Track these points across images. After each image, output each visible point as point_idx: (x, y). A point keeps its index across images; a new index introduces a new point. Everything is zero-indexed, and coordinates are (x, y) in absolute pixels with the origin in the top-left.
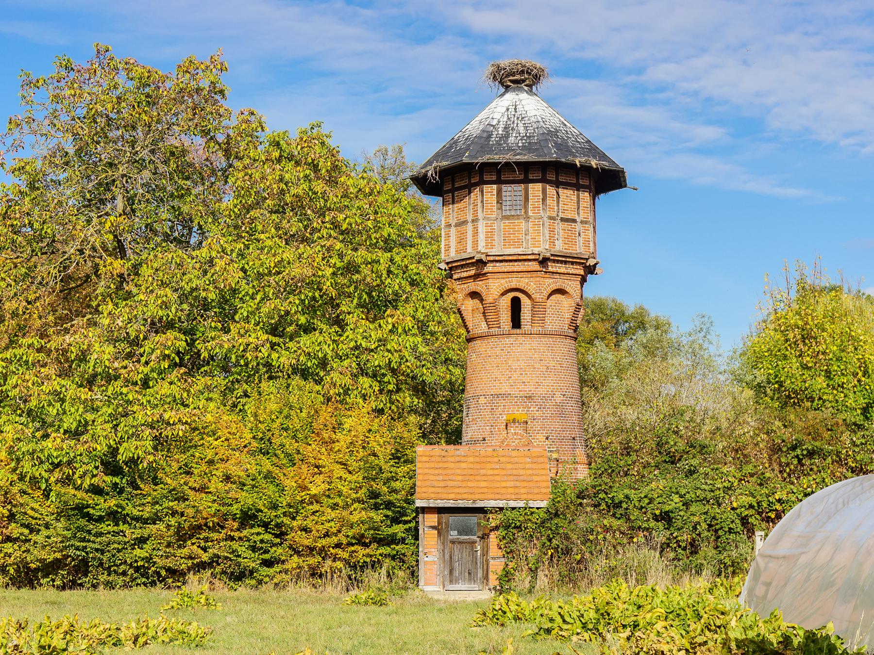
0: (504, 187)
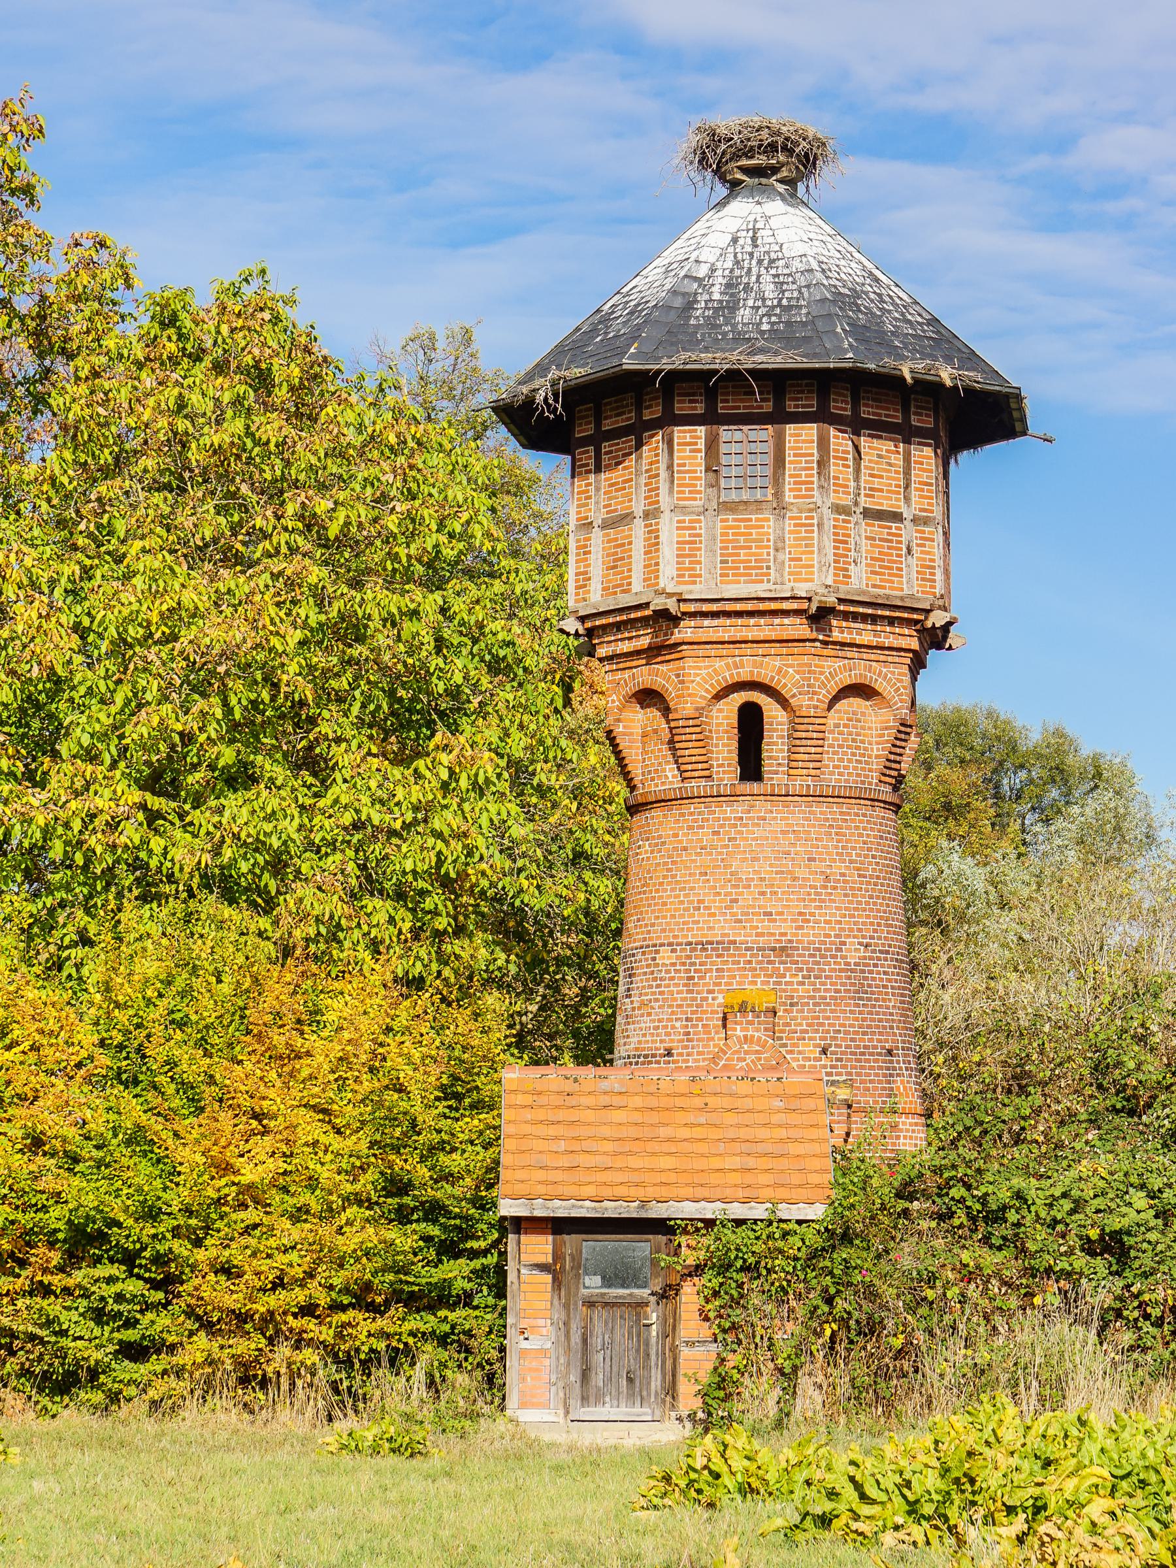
0: (726, 433)
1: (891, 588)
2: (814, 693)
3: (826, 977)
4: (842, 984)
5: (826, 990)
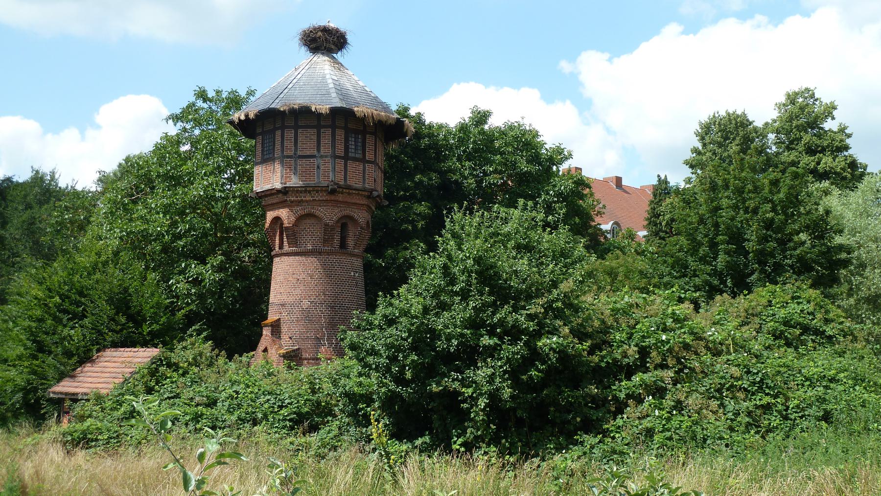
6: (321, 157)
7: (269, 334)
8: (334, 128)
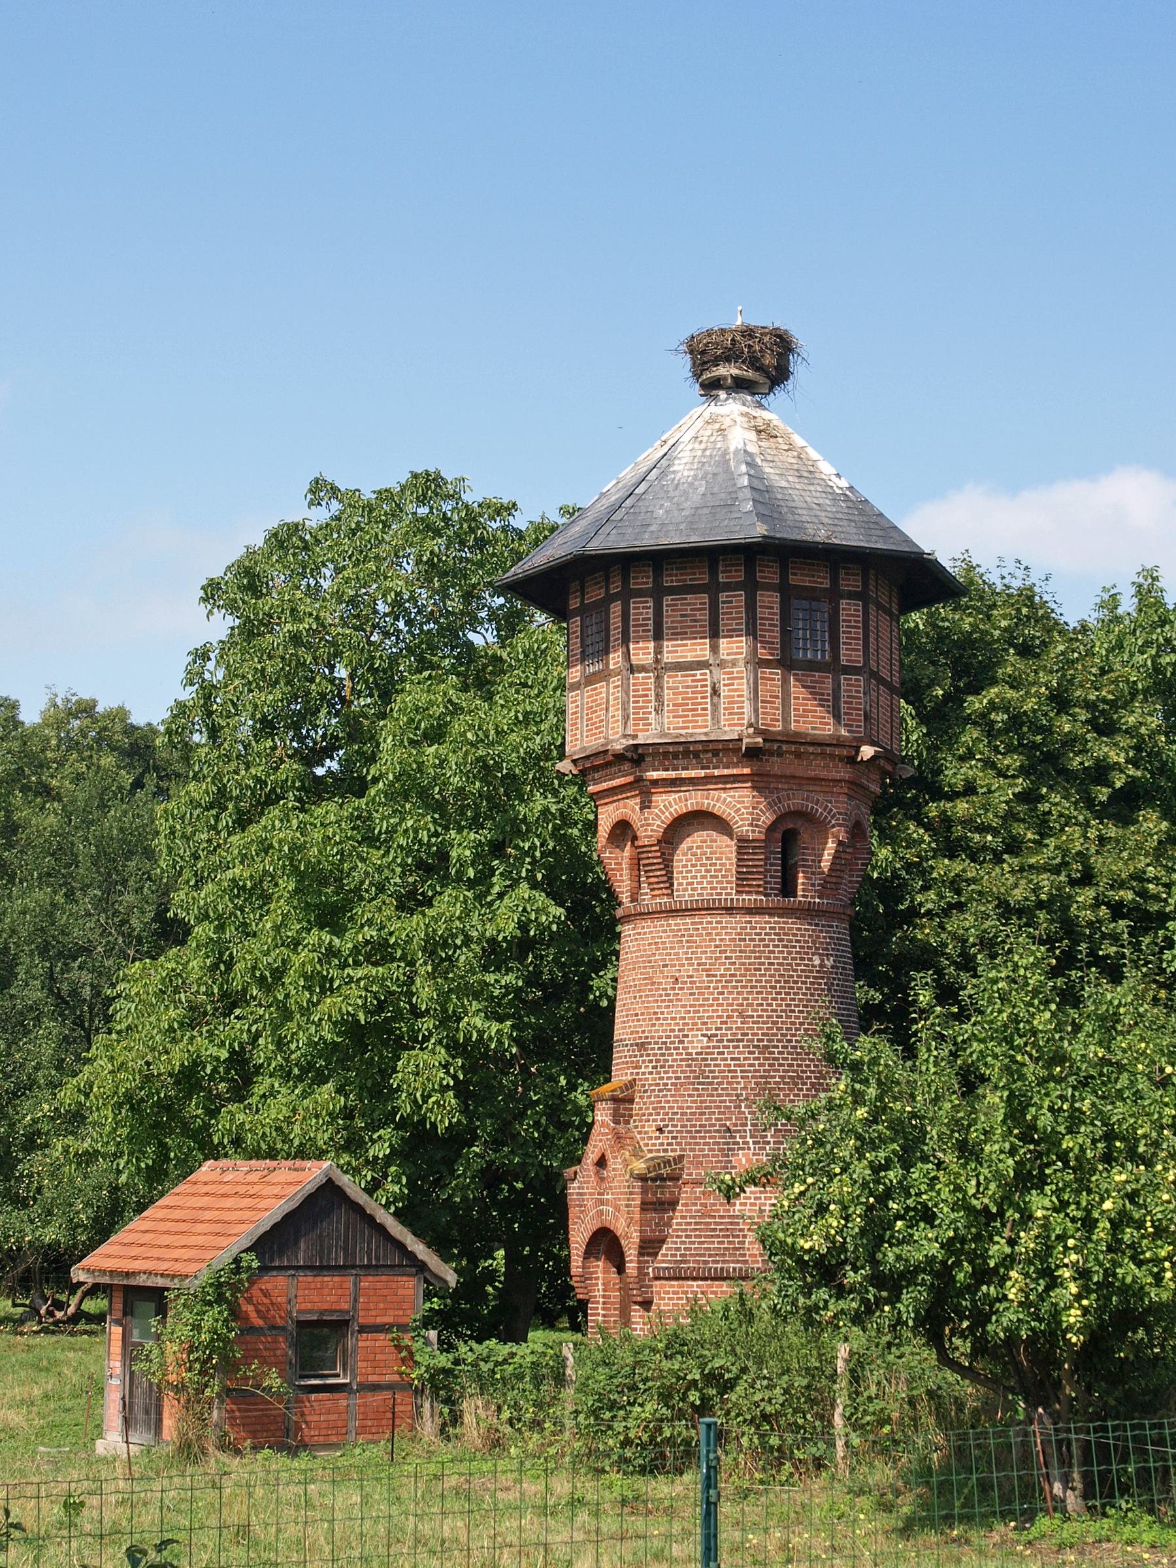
1: (694, 727)
2: (648, 825)
3: (669, 1067)
4: (682, 1072)
5: (668, 1078)
6: (721, 664)
7: (608, 1119)
8: (751, 587)
